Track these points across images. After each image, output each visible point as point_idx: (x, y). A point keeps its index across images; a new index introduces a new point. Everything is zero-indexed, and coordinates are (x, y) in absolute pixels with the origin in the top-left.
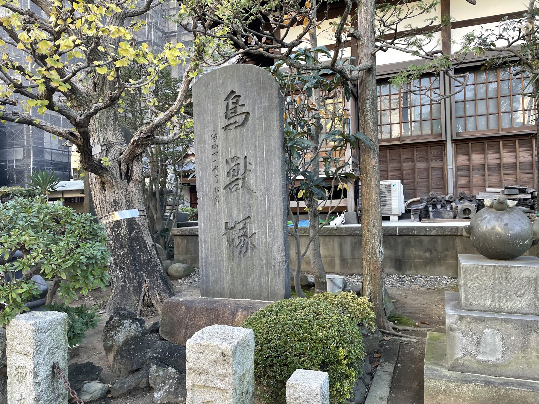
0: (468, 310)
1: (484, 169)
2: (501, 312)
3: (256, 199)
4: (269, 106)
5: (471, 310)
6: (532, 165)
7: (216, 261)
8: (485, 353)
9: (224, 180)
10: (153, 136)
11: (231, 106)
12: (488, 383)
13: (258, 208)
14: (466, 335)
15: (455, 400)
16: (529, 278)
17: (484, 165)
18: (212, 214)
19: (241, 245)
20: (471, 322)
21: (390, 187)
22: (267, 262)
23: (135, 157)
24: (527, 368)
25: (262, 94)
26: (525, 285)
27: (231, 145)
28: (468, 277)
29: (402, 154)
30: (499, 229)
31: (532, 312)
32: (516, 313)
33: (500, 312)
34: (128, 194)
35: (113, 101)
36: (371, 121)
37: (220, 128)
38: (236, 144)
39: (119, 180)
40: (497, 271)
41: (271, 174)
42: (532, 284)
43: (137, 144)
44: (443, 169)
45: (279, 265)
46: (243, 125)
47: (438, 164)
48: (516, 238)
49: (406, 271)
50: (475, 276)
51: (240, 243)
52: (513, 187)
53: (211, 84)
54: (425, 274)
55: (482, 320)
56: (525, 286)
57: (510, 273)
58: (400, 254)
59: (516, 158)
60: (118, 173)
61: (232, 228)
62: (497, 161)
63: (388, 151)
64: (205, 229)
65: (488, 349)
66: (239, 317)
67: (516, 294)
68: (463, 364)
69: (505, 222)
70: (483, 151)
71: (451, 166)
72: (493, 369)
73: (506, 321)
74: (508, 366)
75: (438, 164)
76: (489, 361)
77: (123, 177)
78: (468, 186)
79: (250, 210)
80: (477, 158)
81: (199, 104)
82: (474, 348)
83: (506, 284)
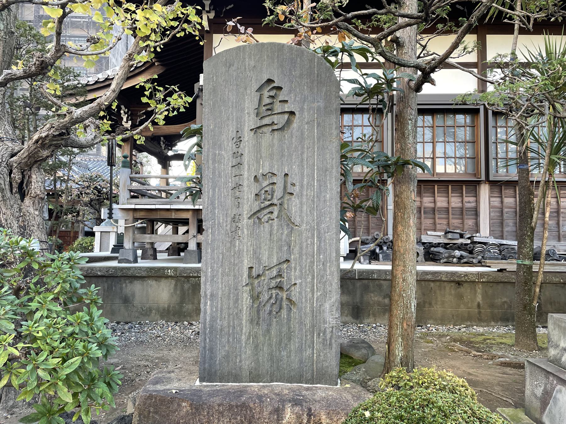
3: (300, 234)
4: (326, 108)
6: (462, 211)
7: (229, 326)
9: (249, 204)
10: (69, 134)
11: (267, 101)
13: (301, 248)
18: (228, 254)
19: (273, 301)
22: (313, 326)
23: (36, 162)
25: (316, 90)
27: (263, 155)
34: (21, 216)
35: (43, 69)
37: (246, 129)
38: (271, 156)
39: (8, 194)
41: (325, 201)
43: (42, 143)
45: (332, 332)
46: (281, 129)
49: (364, 319)
51: (271, 298)
52: (455, 231)
53: (235, 65)
54: (383, 322)
58: (358, 300)
59: (448, 203)
60: (7, 183)
61: (259, 276)
62: (432, 205)
64: (213, 277)
66: (288, 416)
77: (14, 191)
79: (290, 251)
81: (214, 90)
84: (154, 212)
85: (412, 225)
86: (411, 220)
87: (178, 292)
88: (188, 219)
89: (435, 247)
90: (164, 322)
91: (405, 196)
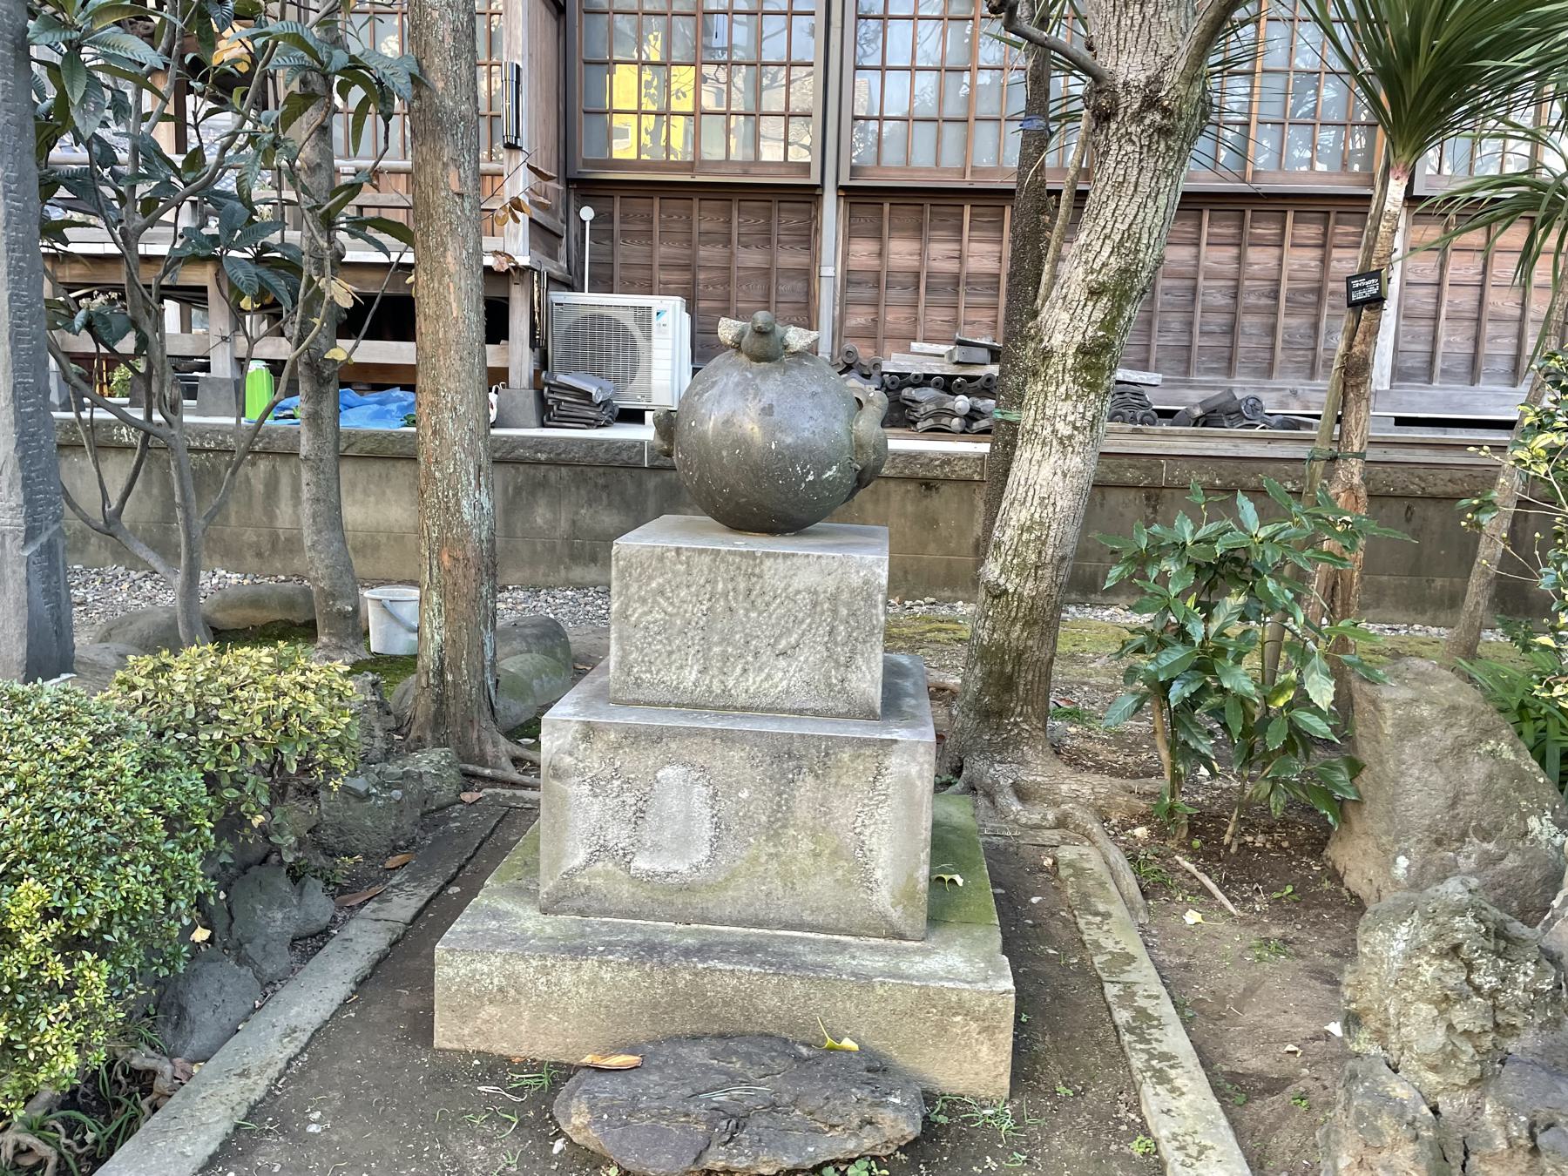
0: (627, 703)
1: (918, 288)
2: (726, 707)
5: (637, 702)
8: (657, 848)
12: (650, 950)
14: (603, 788)
15: (536, 1019)
16: (816, 593)
17: (917, 275)
20: (620, 747)
21: (650, 320)
24: (780, 892)
26: (801, 615)
28: (634, 589)
29: (695, 216)
30: (751, 426)
31: (819, 705)
32: (769, 710)
33: (725, 708)
36: (442, 17)
40: (723, 567)
42: (822, 613)
44: (808, 276)
47: (797, 260)
48: (794, 459)
50: (654, 585)
55: (656, 737)
56: (803, 621)
57: (760, 576)
62: (952, 266)
63: (657, 202)
65: (667, 834)
67: (773, 646)
68: (587, 888)
69: (765, 401)
70: (918, 232)
71: (830, 269)
72: (679, 901)
73: (727, 738)
74: (726, 889)
75: (797, 260)
76: (668, 874)
78: (871, 333)
80: (901, 252)
82: (624, 833)
83: (747, 611)
84: (109, 266)
85: (452, 268)
86: (449, 254)
87: (155, 491)
88: (204, 289)
89: (915, 386)
90: (122, 569)
91: (429, 180)
